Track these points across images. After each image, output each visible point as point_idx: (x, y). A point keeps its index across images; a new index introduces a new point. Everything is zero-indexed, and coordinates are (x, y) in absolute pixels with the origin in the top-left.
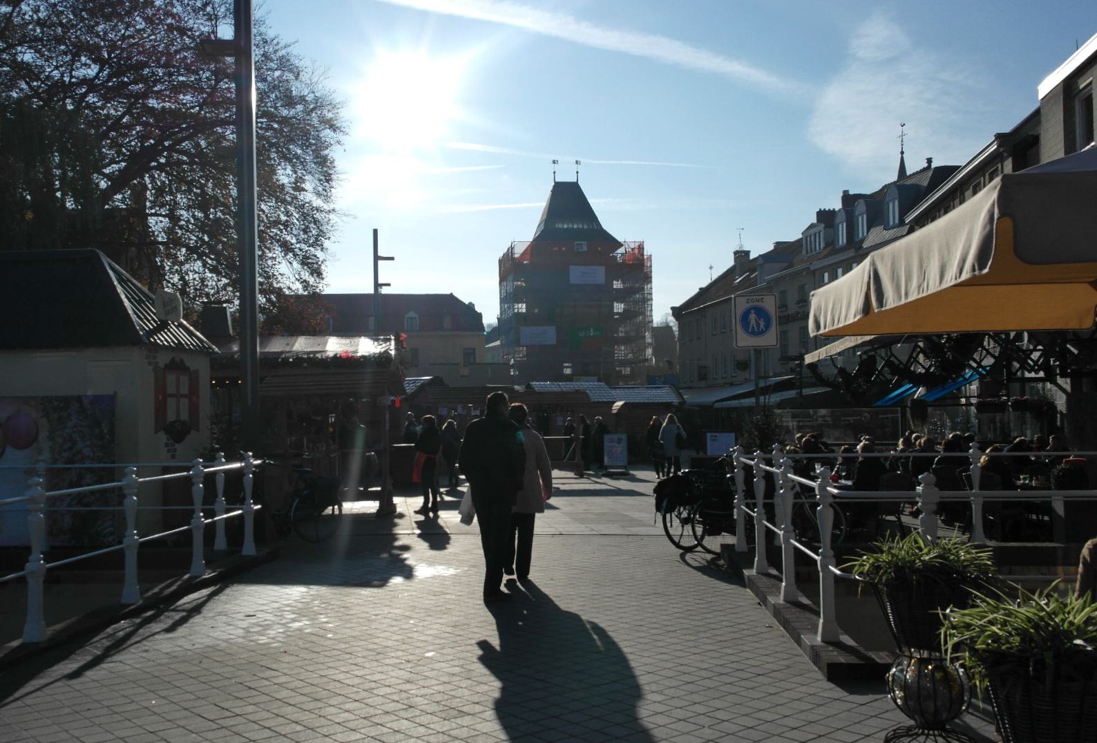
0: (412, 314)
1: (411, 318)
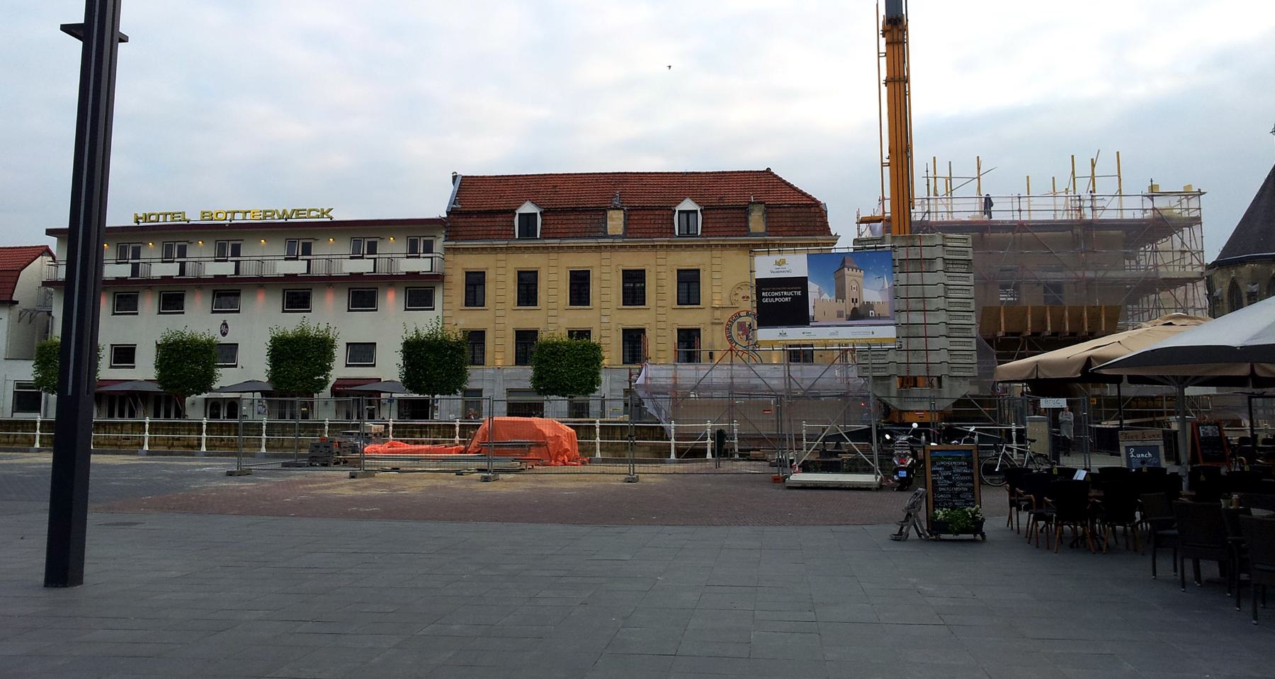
0: (688, 205)
1: (688, 212)
